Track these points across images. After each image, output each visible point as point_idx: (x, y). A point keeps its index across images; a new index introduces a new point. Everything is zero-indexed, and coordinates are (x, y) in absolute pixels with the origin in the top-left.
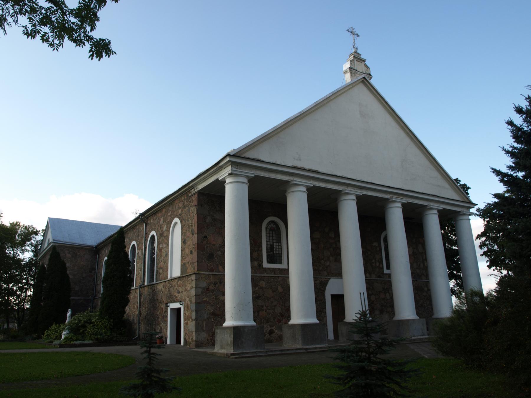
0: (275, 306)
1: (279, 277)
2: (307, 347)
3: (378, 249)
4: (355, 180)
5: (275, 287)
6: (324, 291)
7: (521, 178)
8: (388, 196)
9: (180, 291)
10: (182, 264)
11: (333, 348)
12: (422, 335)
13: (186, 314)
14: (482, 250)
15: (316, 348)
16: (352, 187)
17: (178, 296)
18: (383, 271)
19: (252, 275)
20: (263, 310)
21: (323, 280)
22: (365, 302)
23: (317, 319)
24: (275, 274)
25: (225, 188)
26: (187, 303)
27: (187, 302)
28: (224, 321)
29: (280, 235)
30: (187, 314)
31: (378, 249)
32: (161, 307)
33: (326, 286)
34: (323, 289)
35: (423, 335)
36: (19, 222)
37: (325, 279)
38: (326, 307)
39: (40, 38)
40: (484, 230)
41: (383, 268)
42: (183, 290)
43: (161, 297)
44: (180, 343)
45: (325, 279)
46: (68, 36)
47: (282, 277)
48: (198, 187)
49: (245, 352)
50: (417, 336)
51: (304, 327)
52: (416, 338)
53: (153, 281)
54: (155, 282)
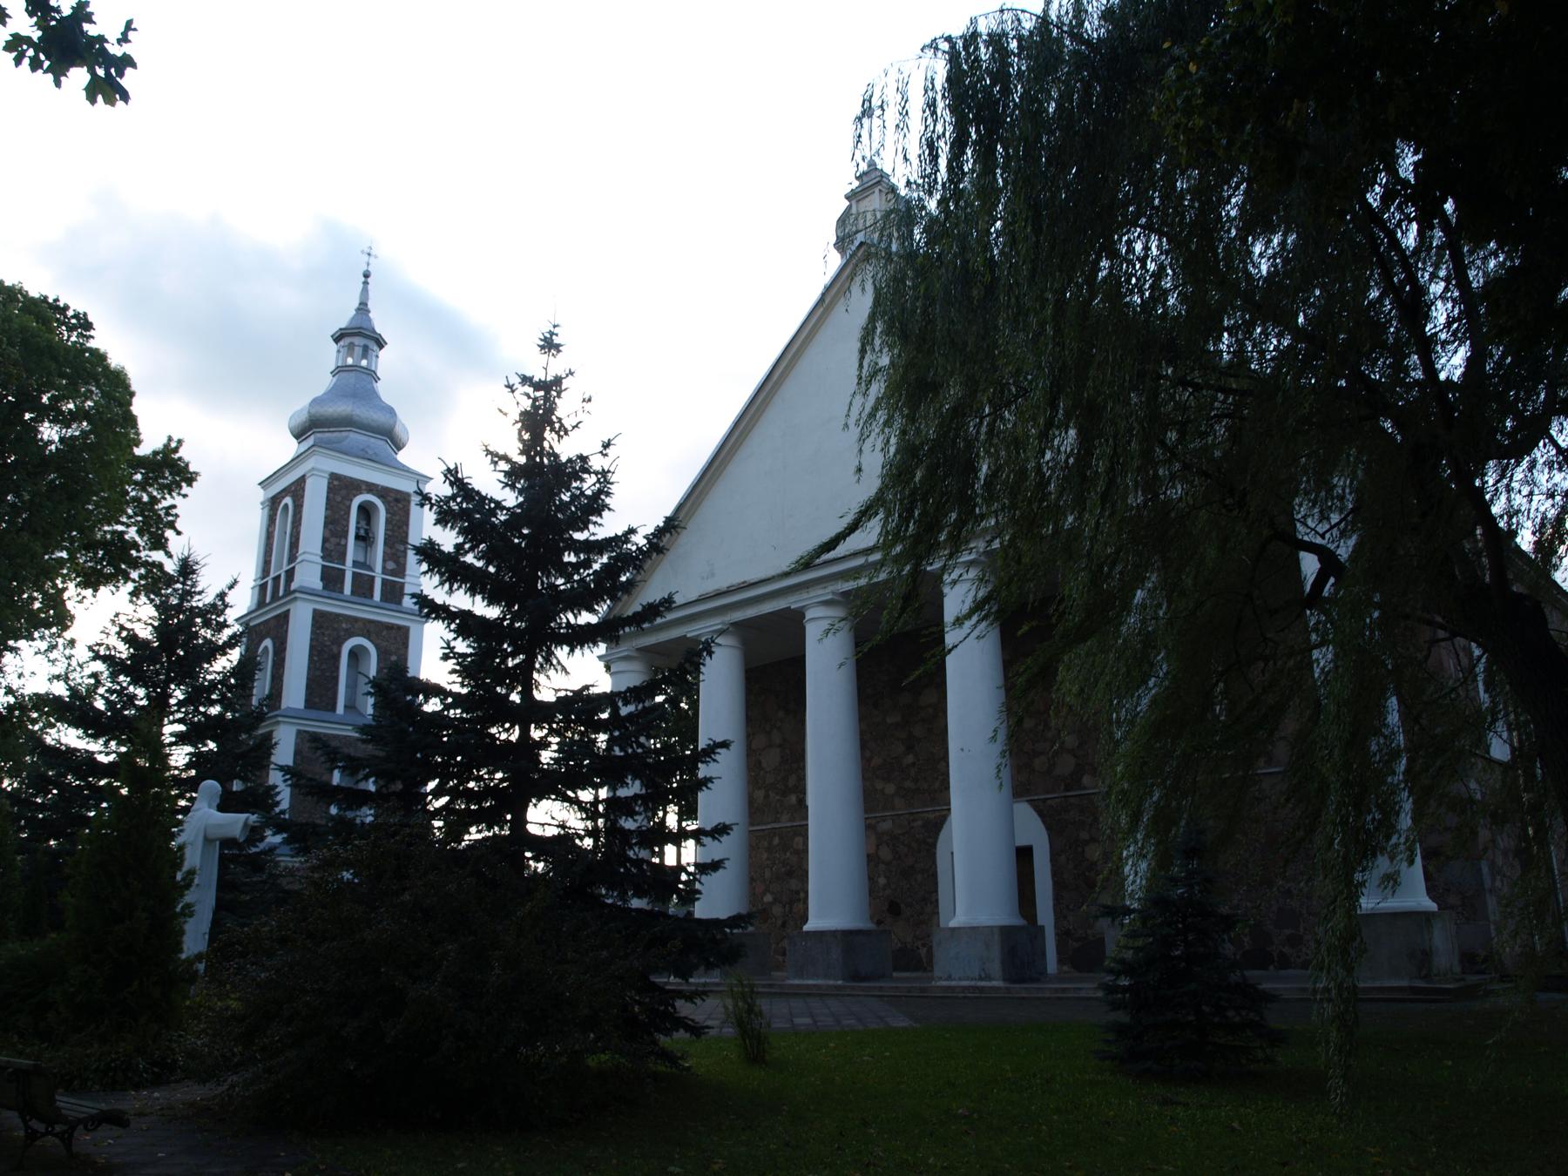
4: (843, 557)
6: (934, 845)
7: (67, 699)
8: (268, 730)
12: (981, 979)
15: (1064, 990)
16: (817, 584)
19: (751, 829)
20: (799, 900)
21: (932, 816)
23: (1430, 898)
25: (803, 629)
28: (806, 920)
33: (940, 831)
34: (930, 840)
35: (989, 978)
37: (937, 814)
38: (940, 889)
39: (228, 611)
40: (1319, 566)
45: (937, 814)
46: (1416, 158)
50: (960, 979)
51: (847, 938)
52: (953, 983)
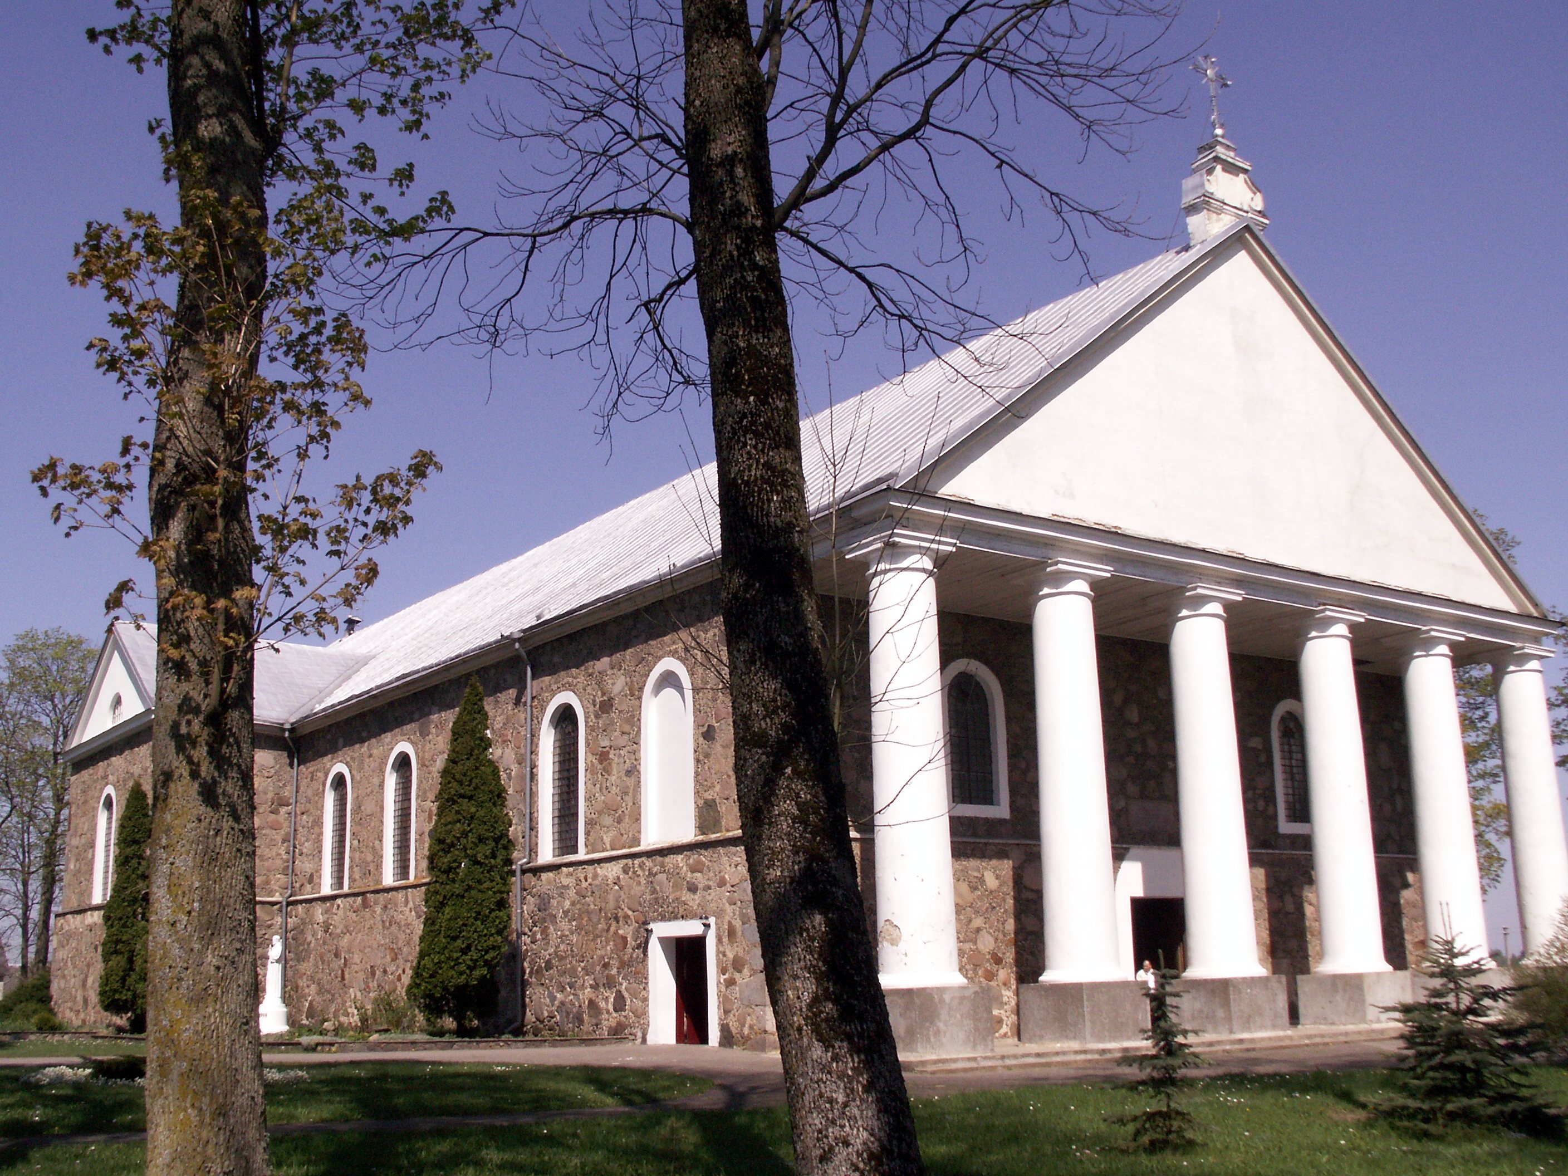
0: (978, 930)
1: (986, 844)
2: (1101, 1046)
3: (1263, 758)
5: (976, 874)
9: (701, 886)
10: (701, 802)
11: (1228, 1047)
13: (724, 955)
14: (68, 465)
17: (693, 900)
18: (1276, 827)
22: (1519, 935)
24: (975, 835)
26: (730, 922)
27: (727, 918)
29: (987, 715)
30: (730, 955)
31: (1263, 758)
32: (616, 933)
36: (21, 649)
41: (1275, 817)
42: (711, 883)
43: (617, 901)
44: (704, 1039)
47: (994, 844)
48: (708, 550)
49: (944, 1057)
53: (575, 850)
54: (582, 855)
